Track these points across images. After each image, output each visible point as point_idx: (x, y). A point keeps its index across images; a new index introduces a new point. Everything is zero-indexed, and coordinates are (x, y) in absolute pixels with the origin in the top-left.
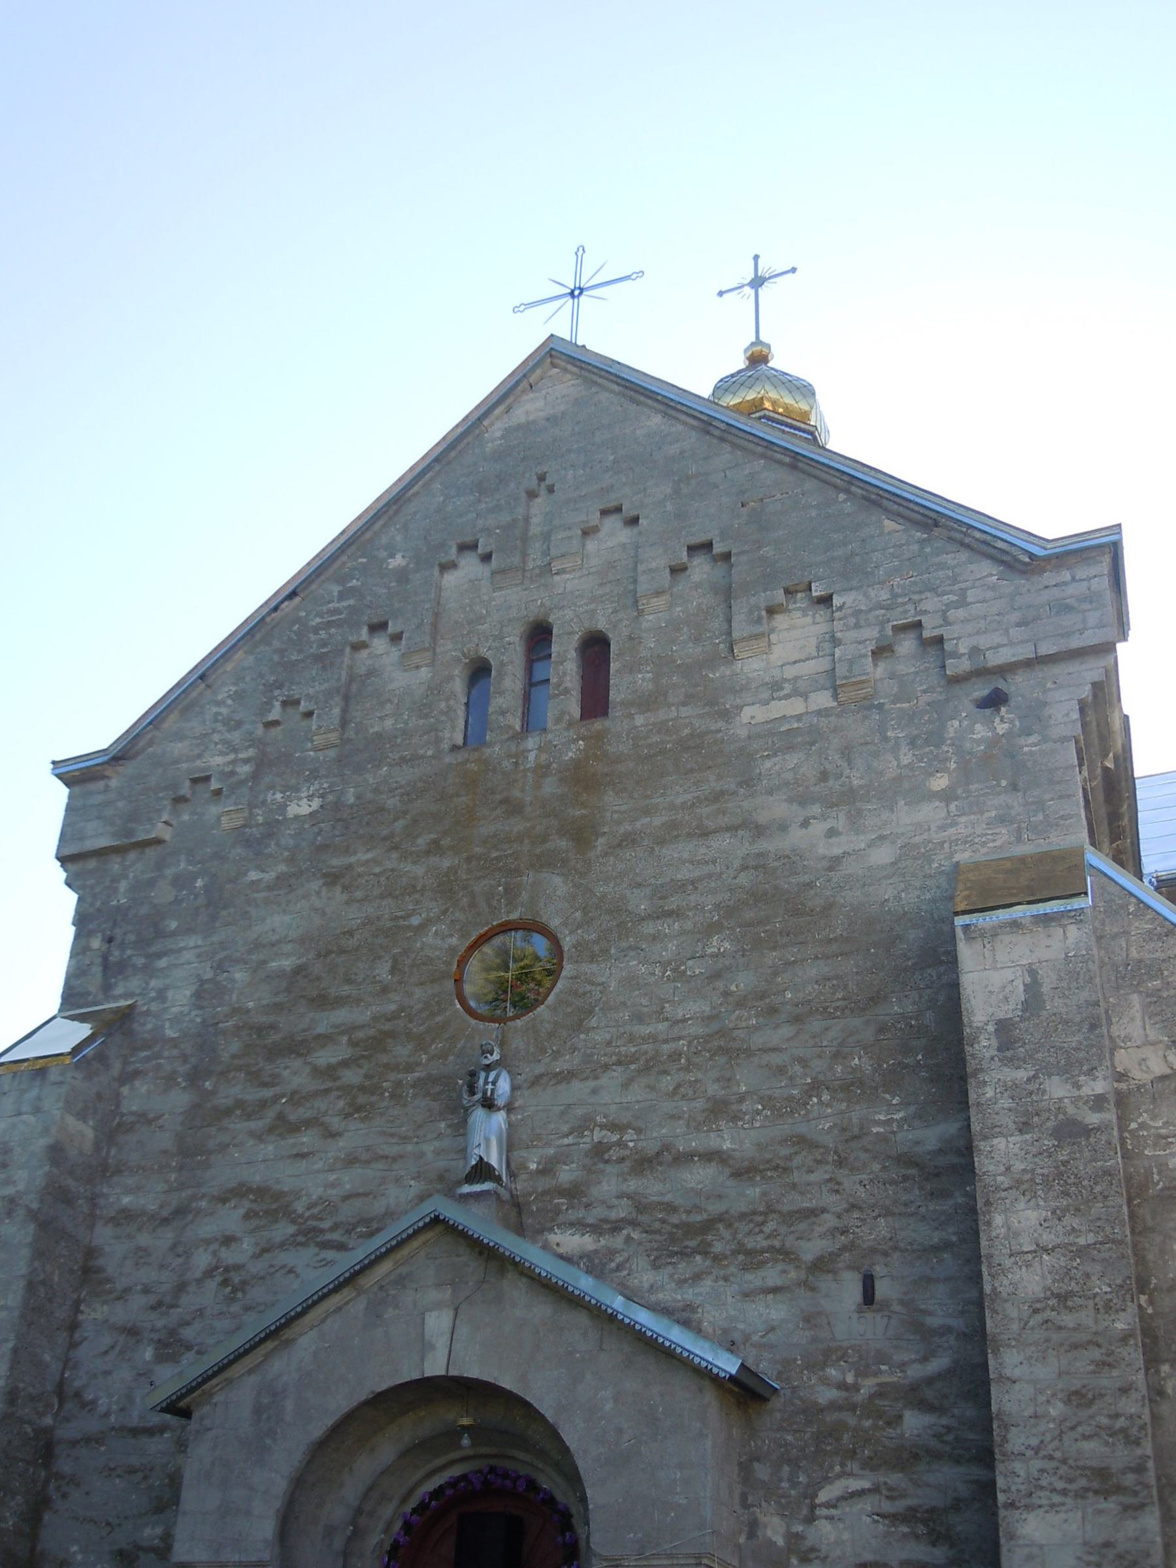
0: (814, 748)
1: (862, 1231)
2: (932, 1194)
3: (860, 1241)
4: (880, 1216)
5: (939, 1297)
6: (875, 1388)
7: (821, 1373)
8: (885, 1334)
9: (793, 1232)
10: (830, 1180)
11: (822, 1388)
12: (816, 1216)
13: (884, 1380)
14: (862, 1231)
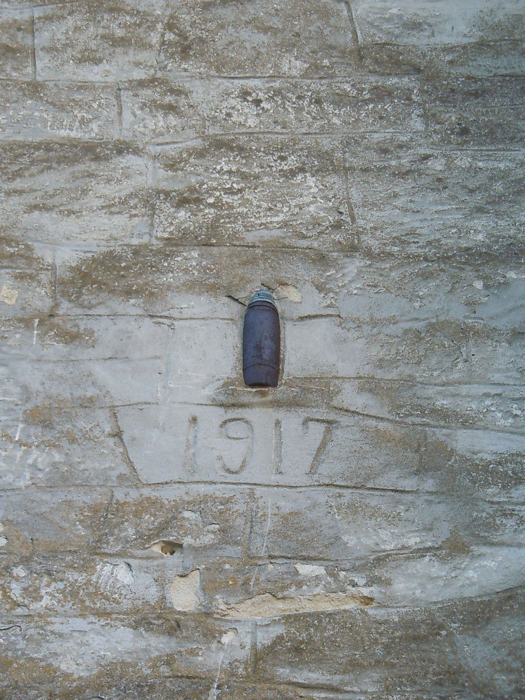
0: (37, 153)
1: (246, 202)
2: (464, 131)
3: (239, 226)
4: (302, 170)
5: (497, 377)
6: (280, 630)
7: (80, 578)
8: (312, 471)
9: (20, 192)
10: (151, 82)
11: (80, 623)
12: (97, 158)
13: (309, 607)
14: (246, 202)
